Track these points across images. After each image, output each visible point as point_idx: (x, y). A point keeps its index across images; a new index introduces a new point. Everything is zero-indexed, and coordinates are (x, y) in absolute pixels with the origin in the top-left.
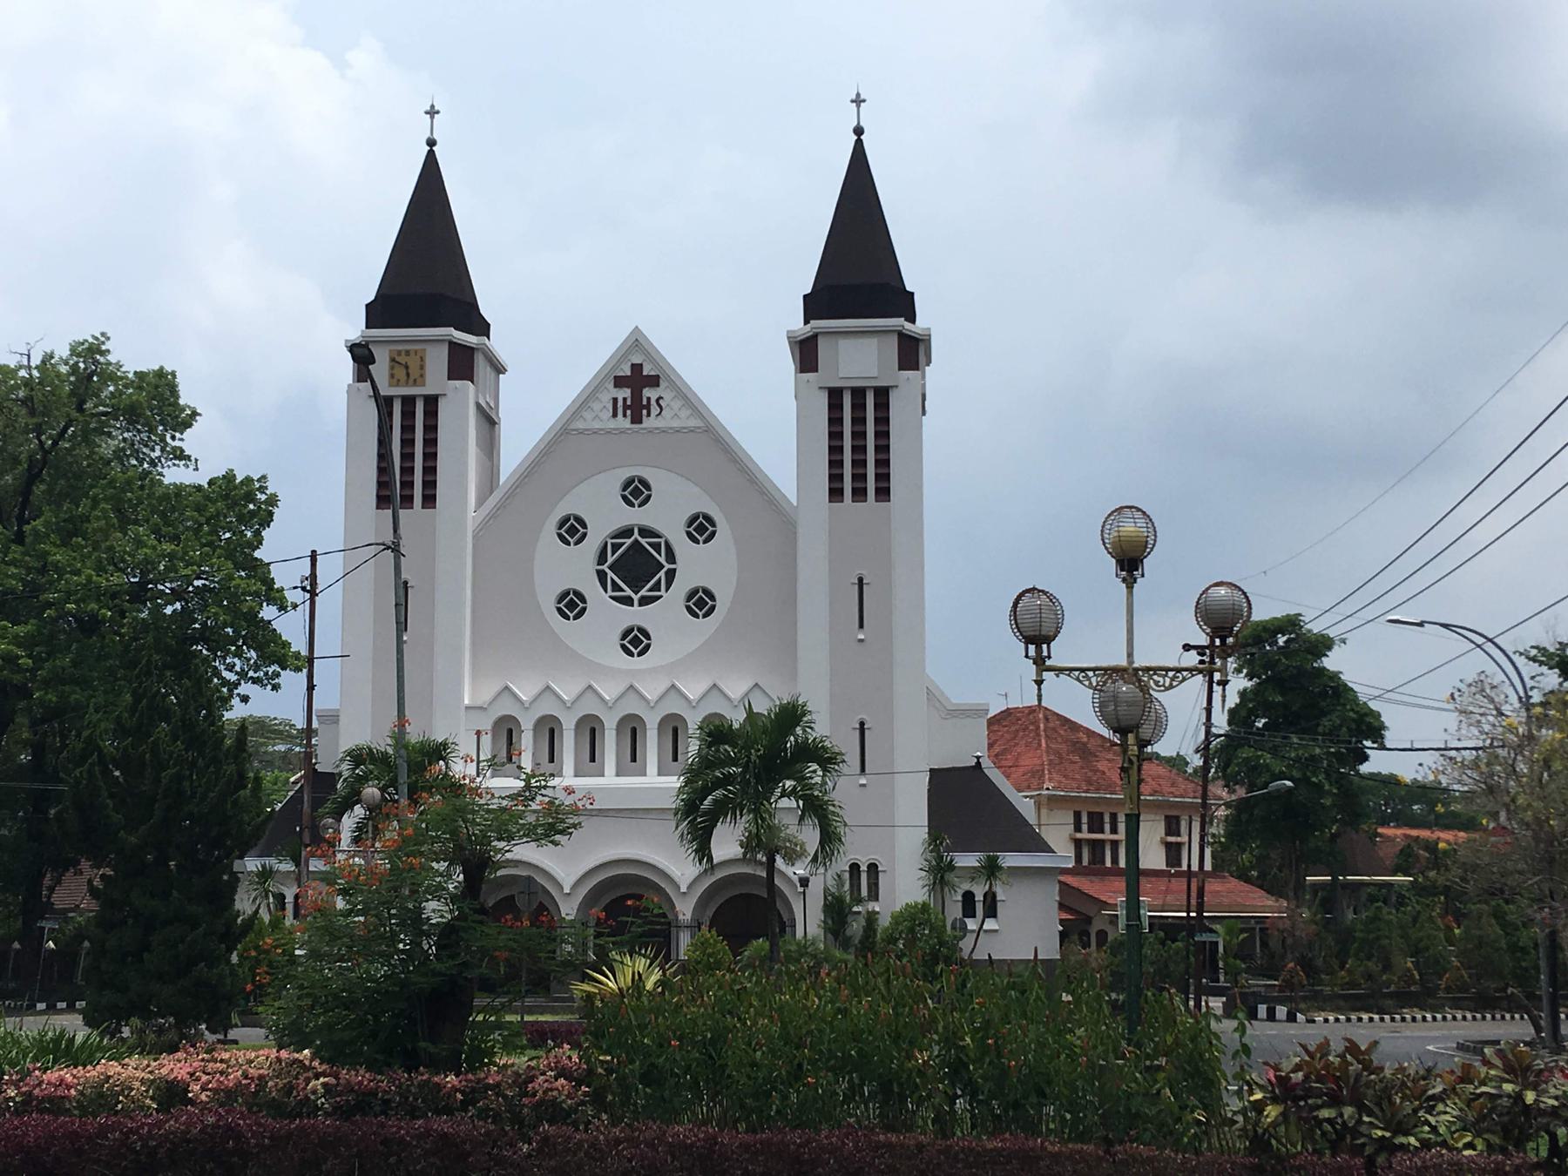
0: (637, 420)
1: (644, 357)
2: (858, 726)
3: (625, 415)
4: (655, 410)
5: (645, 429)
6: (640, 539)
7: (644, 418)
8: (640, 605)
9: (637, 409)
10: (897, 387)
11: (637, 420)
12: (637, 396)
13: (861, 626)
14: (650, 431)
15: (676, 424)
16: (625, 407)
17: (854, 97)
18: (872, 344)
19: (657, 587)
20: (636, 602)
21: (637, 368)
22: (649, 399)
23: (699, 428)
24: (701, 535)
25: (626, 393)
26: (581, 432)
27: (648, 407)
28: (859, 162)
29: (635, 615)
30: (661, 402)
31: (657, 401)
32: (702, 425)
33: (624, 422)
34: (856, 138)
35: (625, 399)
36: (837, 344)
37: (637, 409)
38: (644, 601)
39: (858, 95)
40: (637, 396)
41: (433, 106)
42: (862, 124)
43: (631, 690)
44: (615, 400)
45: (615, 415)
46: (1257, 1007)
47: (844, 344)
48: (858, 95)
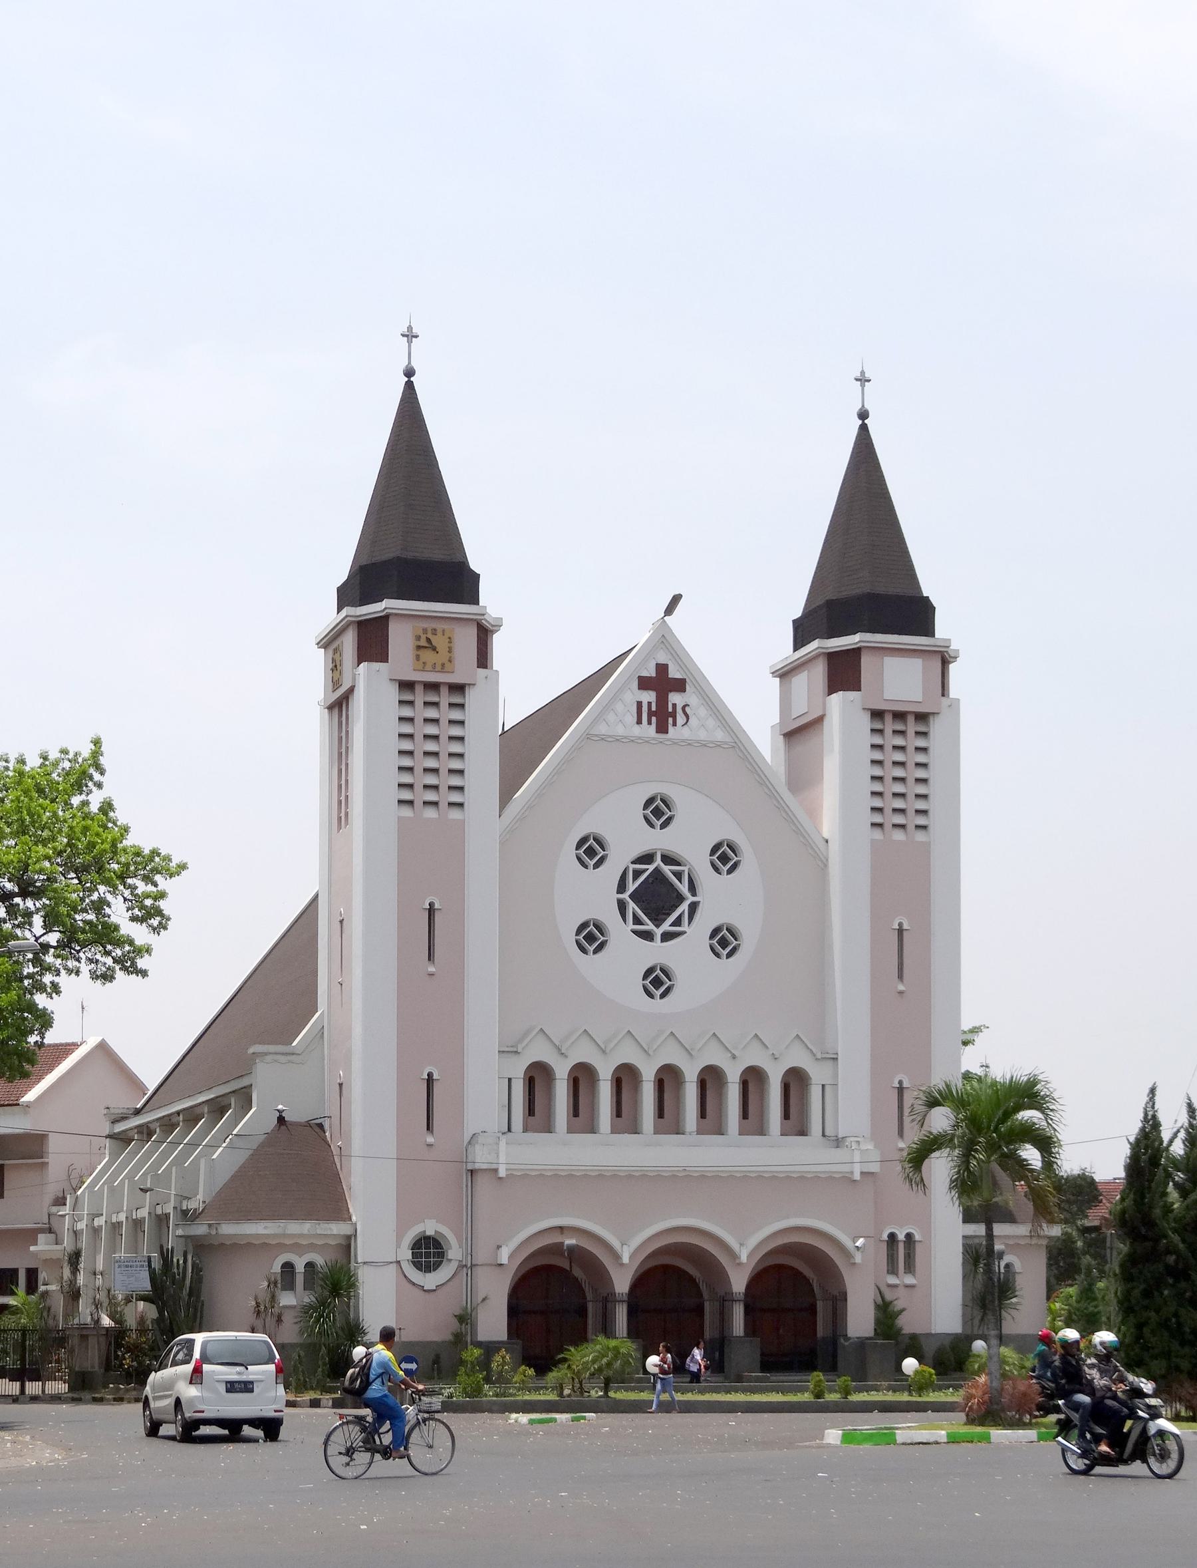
0: (662, 729)
1: (670, 657)
2: (693, 1053)
3: (650, 723)
4: (680, 719)
5: (668, 740)
6: (662, 865)
7: (671, 728)
8: (662, 941)
9: (662, 717)
10: (938, 713)
11: (662, 729)
12: (662, 700)
13: (900, 976)
14: (675, 743)
15: (702, 735)
16: (651, 714)
17: (858, 375)
18: (916, 663)
19: (678, 922)
20: (658, 938)
21: (662, 669)
22: (674, 705)
23: (726, 743)
24: (724, 865)
25: (649, 697)
26: (603, 738)
27: (674, 715)
28: (864, 454)
29: (656, 953)
30: (687, 709)
31: (683, 709)
32: (728, 739)
33: (650, 730)
34: (860, 422)
35: (650, 704)
36: (883, 659)
37: (662, 717)
38: (667, 937)
39: (410, 328)
40: (662, 700)
41: (863, 373)
42: (866, 406)
43: (830, 1063)
44: (639, 704)
45: (639, 722)
46: (630, 1261)
47: (892, 664)
48: (410, 328)
